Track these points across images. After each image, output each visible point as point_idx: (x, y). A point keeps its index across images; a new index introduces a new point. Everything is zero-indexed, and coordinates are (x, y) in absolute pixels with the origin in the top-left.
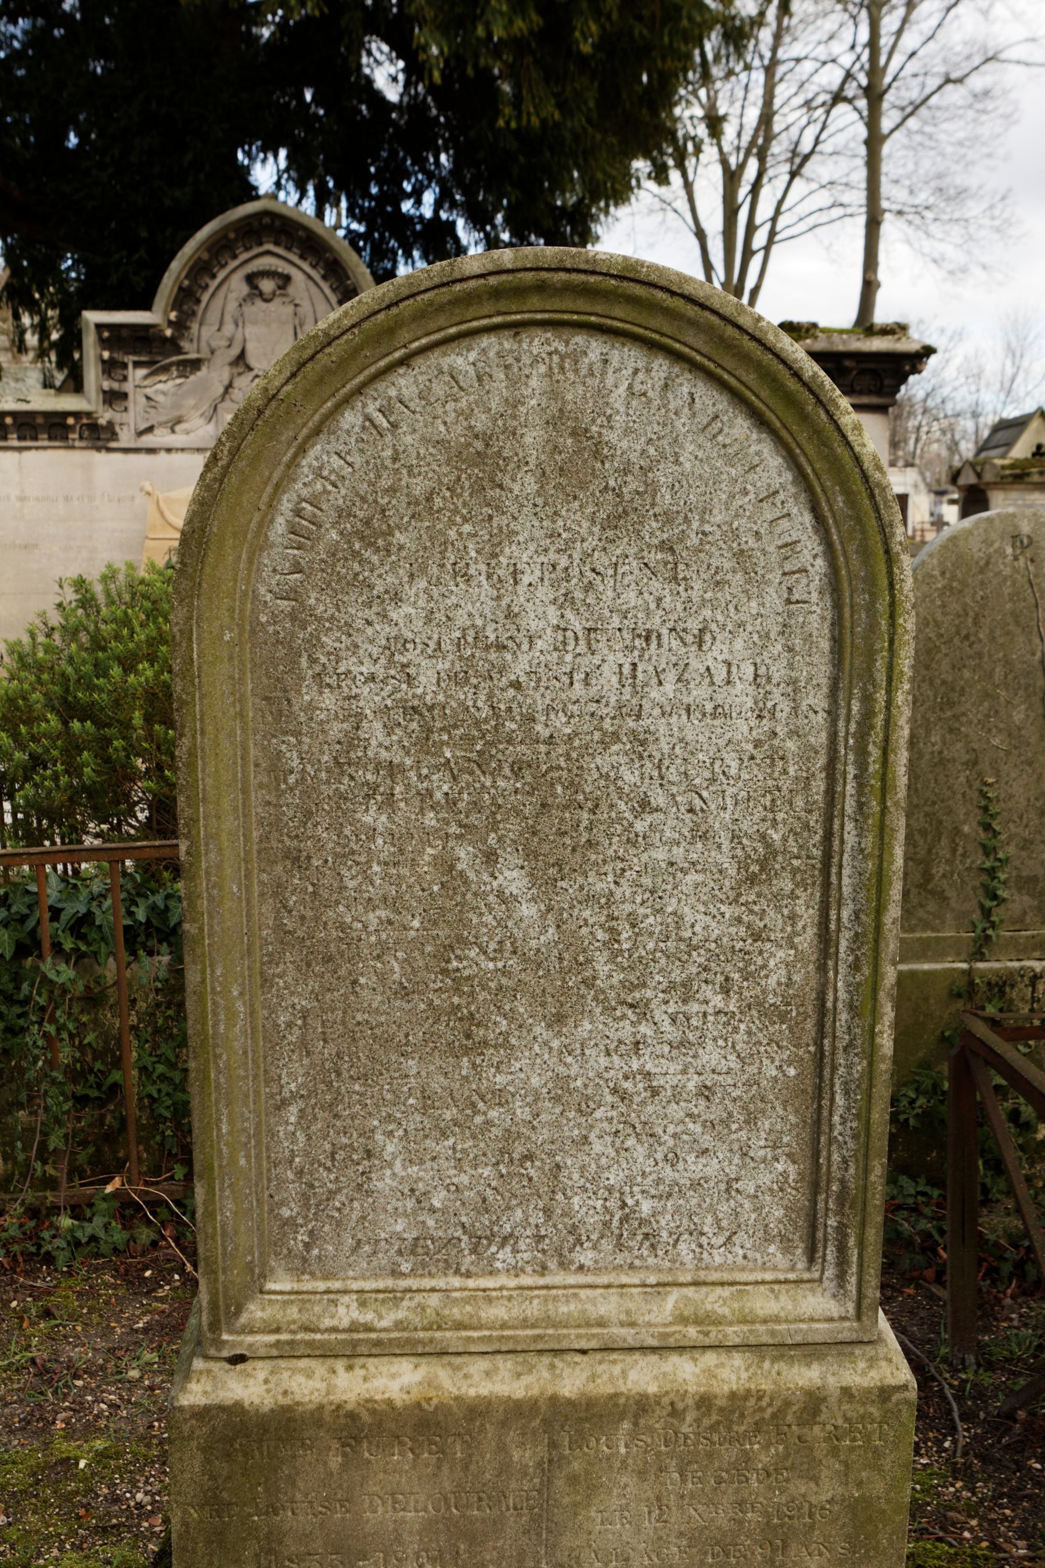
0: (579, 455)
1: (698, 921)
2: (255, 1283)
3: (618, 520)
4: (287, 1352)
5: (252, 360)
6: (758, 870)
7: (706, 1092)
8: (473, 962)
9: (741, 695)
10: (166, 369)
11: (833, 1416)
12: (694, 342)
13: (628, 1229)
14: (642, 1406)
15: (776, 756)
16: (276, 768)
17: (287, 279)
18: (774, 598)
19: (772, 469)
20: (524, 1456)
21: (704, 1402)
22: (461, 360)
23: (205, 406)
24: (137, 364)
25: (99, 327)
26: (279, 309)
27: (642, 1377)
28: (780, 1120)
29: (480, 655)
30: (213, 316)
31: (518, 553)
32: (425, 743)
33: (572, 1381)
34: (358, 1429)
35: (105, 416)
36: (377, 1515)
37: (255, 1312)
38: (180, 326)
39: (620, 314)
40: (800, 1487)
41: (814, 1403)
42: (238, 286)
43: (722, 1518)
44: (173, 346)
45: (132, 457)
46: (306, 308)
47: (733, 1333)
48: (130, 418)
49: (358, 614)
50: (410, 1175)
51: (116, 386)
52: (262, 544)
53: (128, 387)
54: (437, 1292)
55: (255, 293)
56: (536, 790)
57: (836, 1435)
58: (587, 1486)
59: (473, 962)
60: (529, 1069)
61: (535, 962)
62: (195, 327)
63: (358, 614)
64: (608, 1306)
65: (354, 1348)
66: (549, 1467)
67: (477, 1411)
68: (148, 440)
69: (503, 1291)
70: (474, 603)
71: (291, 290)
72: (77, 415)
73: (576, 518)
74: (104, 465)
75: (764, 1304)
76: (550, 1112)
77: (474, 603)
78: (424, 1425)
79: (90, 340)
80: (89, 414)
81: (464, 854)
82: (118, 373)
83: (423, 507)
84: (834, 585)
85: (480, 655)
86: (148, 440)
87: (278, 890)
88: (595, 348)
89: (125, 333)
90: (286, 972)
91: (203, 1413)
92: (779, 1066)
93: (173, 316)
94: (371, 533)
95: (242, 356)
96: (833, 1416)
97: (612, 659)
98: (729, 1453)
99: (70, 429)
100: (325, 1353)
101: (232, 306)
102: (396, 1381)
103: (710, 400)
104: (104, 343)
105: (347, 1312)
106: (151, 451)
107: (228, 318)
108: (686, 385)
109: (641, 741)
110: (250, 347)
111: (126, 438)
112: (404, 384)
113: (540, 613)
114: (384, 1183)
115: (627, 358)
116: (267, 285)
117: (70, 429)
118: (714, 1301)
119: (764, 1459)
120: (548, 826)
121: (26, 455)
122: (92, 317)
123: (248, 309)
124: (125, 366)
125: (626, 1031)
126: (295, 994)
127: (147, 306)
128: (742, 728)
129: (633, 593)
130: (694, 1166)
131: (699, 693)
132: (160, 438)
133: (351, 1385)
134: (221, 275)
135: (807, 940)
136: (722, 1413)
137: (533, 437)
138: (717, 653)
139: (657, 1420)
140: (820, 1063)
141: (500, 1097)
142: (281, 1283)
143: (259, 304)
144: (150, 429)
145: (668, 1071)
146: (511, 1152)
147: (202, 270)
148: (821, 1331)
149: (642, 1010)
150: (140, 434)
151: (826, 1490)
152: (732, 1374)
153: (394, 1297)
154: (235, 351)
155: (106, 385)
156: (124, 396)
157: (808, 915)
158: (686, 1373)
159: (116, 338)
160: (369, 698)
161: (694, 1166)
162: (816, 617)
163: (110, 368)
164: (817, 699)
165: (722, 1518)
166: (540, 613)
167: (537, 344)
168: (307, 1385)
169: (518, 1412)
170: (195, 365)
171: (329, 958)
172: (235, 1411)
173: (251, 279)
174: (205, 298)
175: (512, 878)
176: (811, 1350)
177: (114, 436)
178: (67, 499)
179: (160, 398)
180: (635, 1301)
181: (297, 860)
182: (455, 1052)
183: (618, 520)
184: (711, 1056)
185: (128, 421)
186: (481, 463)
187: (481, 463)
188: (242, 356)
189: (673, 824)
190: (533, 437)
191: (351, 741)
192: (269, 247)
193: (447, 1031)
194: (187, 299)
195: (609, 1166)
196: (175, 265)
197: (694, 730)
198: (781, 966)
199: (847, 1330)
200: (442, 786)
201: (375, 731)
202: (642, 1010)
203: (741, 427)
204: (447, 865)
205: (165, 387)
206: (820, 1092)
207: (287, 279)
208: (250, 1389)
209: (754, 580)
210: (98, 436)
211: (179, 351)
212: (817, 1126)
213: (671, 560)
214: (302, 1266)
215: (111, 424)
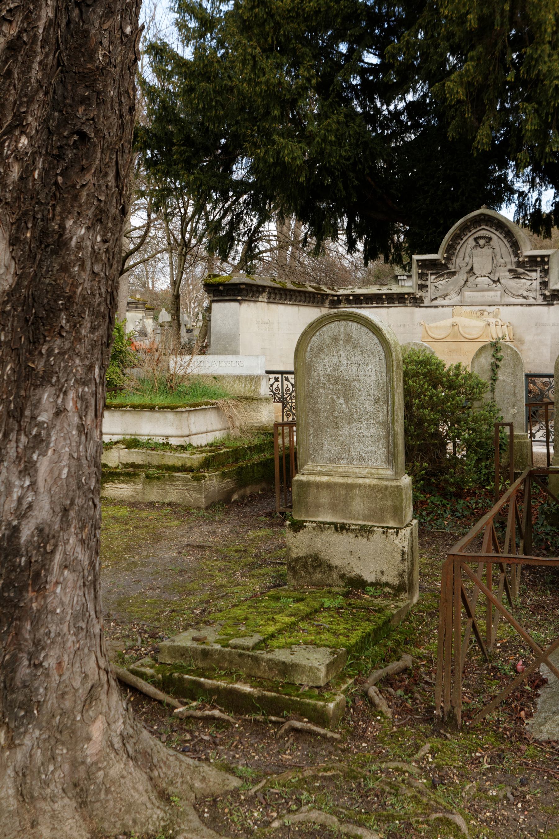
0: (349, 339)
1: (369, 409)
2: (306, 463)
3: (354, 347)
4: (310, 474)
5: (475, 271)
6: (377, 401)
7: (371, 436)
8: (337, 414)
9: (373, 373)
10: (442, 275)
11: (390, 490)
12: (363, 322)
13: (361, 458)
14: (360, 485)
15: (379, 383)
16: (309, 383)
17: (490, 239)
18: (377, 359)
19: (376, 340)
20: (343, 492)
21: (369, 486)
22: (332, 325)
23: (457, 289)
24: (432, 274)
25: (418, 261)
26: (487, 251)
27: (361, 481)
28: (383, 441)
29: (336, 367)
30: (461, 255)
31: (341, 352)
32: (329, 380)
33: (350, 481)
34: (319, 485)
35: (419, 294)
36: (322, 500)
37: (306, 467)
38: (448, 259)
39: (353, 319)
40: (385, 502)
41: (386, 487)
42: (471, 242)
43: (373, 506)
44: (445, 267)
45: (429, 309)
46: (497, 250)
47: (376, 476)
48: (428, 294)
49: (319, 361)
50: (329, 447)
51: (423, 282)
52: (306, 351)
53: (428, 283)
54: (332, 467)
55: (478, 245)
56: (345, 388)
57: (390, 493)
58: (352, 498)
59: (337, 414)
60: (345, 431)
61: (345, 414)
62: (454, 259)
63: (319, 361)
64: (357, 470)
65: (319, 474)
66: (347, 495)
67: (336, 484)
68: (435, 303)
69: (342, 467)
70: (335, 359)
71: (492, 243)
72: (408, 294)
73: (349, 347)
74: (418, 311)
75: (381, 472)
76: (348, 438)
77: (335, 359)
78: (328, 486)
79: (414, 265)
80: (413, 294)
81: (335, 397)
82: (425, 278)
83: (328, 346)
84: (385, 357)
85: (336, 367)
86: (435, 303)
87: (309, 402)
88: (350, 323)
89: (427, 263)
90: (310, 414)
91: (297, 481)
92: (382, 433)
93: (445, 255)
94: (321, 350)
95: (472, 269)
96: (390, 490)
97: (354, 368)
98: (374, 495)
99: (406, 299)
100: (315, 474)
101: (469, 250)
102: (325, 479)
103: (366, 330)
104: (419, 267)
105: (319, 468)
106: (436, 307)
107: (467, 255)
108: (363, 328)
109: (359, 380)
110: (475, 266)
111: (427, 302)
112: (325, 329)
113: (344, 361)
114: (325, 448)
115: (355, 324)
116: (482, 242)
117: (406, 299)
118: (373, 471)
119: (379, 496)
120: (347, 393)
121: (390, 309)
122: (416, 257)
123: (474, 251)
124: (427, 275)
125: (359, 426)
126: (311, 418)
127: (436, 252)
128: (374, 378)
129: (357, 358)
130: (370, 449)
131: (367, 373)
132: (440, 302)
133: (318, 479)
134: (465, 239)
135: (385, 412)
136: (373, 488)
137: (342, 336)
138: (369, 367)
139: (362, 488)
140: (388, 432)
141: (341, 435)
142: (310, 463)
143: (479, 249)
144: (436, 298)
145: (366, 433)
146: (343, 444)
147: (457, 237)
148: (389, 477)
149: (361, 422)
150: (432, 300)
151: (389, 503)
152: (375, 482)
153: (326, 467)
154: (469, 268)
155: (419, 283)
156: (427, 286)
157: (385, 408)
158: (367, 481)
159: (423, 264)
160: (321, 373)
161: (370, 449)
162: (383, 362)
163: (422, 276)
164: (384, 374)
165: (373, 506)
166: (344, 361)
167: (342, 323)
168: (312, 478)
169: (342, 485)
170: (454, 273)
171: (316, 412)
172: (301, 481)
173: (476, 239)
174: (458, 248)
175: (342, 401)
176: (387, 479)
177: (422, 301)
178: (404, 325)
179: (440, 287)
180: (361, 470)
181: (312, 397)
182: (334, 428)
183: (354, 347)
184: (372, 430)
185: (428, 296)
186: (335, 339)
187: (335, 339)
188: (472, 269)
189: (365, 393)
190: (342, 336)
191: (319, 380)
192: (484, 227)
193: (333, 424)
194: (451, 249)
195: (358, 448)
196: (447, 236)
197: (367, 379)
198: (381, 416)
199: (393, 477)
200: (331, 387)
201: (322, 378)
202: (361, 422)
203: (371, 334)
204: (332, 398)
205: (442, 282)
206: (388, 437)
207: (490, 239)
208: (304, 478)
209: (374, 357)
210: (416, 301)
211: (448, 268)
212: (388, 443)
213: (362, 353)
214: (313, 461)
215: (421, 297)
